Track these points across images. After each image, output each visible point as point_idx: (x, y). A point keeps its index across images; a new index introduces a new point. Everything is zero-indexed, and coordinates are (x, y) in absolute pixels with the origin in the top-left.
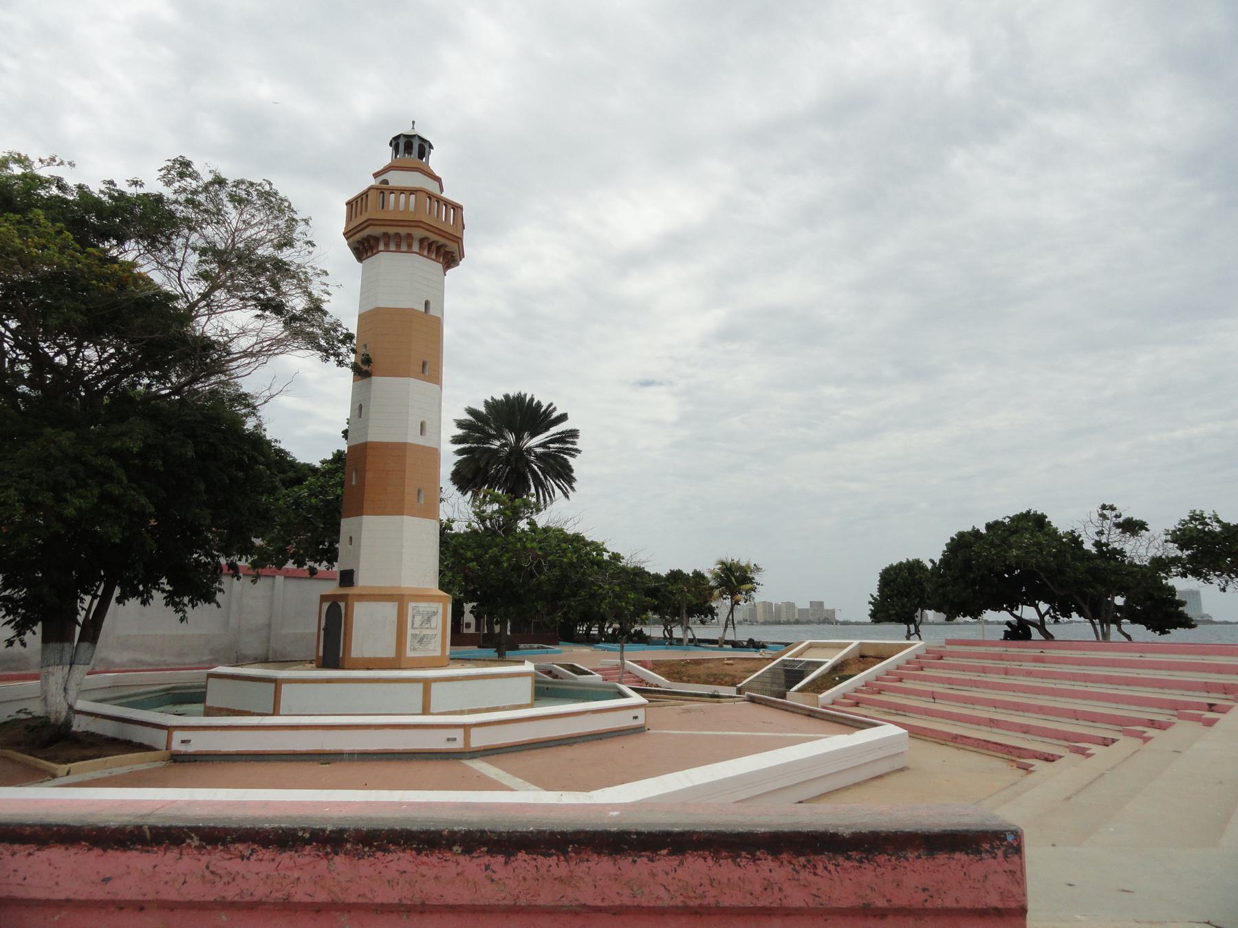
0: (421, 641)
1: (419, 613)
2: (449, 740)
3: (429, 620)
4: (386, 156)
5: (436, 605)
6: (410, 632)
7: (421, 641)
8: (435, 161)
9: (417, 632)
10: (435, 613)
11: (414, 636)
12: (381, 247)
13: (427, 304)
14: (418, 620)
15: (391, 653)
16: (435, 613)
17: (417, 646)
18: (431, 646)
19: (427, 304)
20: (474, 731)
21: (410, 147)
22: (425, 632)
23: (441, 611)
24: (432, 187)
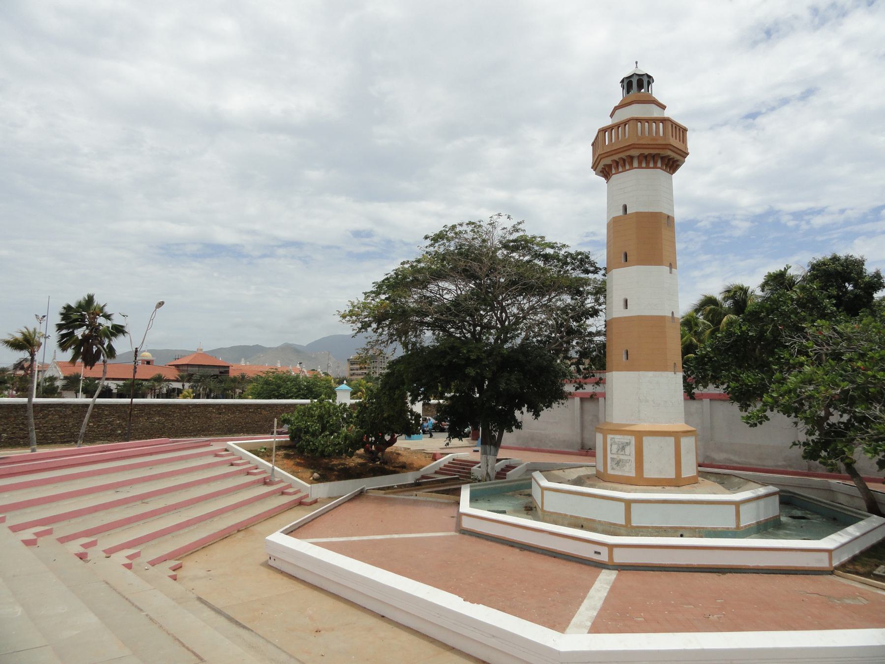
0: (618, 463)
1: (615, 443)
2: (596, 552)
3: (623, 448)
4: (618, 95)
5: (629, 437)
6: (609, 456)
7: (618, 463)
8: (657, 91)
9: (615, 456)
10: (628, 444)
11: (613, 459)
12: (613, 172)
13: (673, 313)
14: (615, 447)
15: (672, 475)
16: (628, 444)
17: (615, 466)
18: (627, 468)
19: (673, 313)
20: (616, 550)
21: (637, 85)
22: (622, 457)
23: (633, 442)
24: (656, 113)
